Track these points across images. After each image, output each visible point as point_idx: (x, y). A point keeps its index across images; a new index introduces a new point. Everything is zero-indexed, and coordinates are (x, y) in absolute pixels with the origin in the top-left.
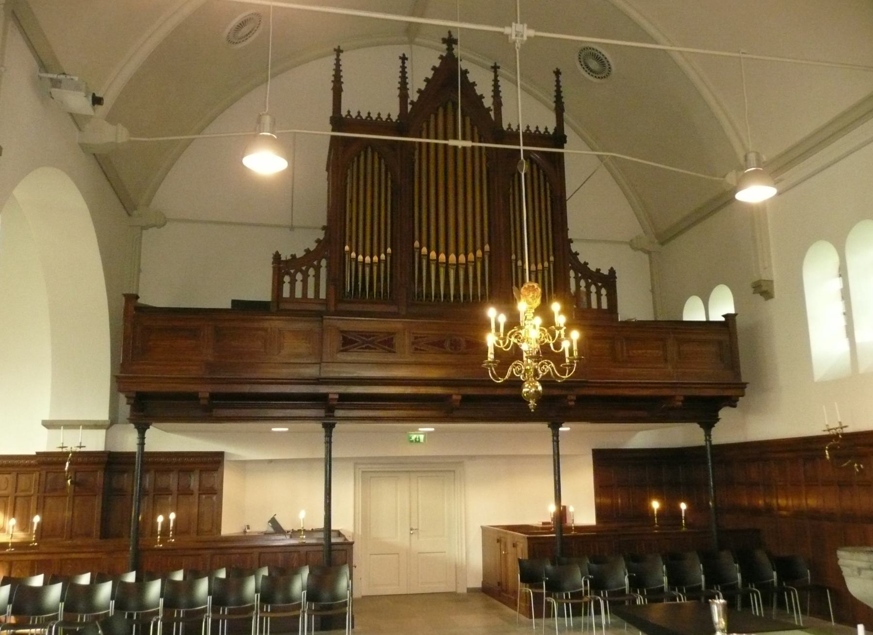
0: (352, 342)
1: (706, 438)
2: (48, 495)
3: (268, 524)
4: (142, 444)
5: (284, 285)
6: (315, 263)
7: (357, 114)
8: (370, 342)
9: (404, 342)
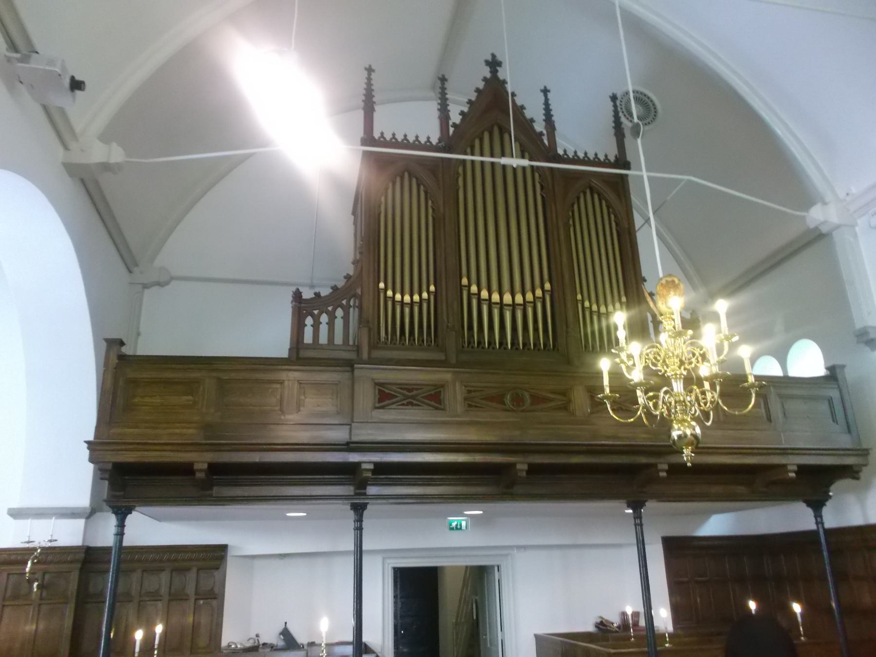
0: (390, 396)
1: (816, 520)
2: (7, 603)
3: (280, 638)
4: (120, 534)
5: (306, 328)
6: (344, 302)
7: (391, 136)
8: (413, 397)
9: (455, 395)
